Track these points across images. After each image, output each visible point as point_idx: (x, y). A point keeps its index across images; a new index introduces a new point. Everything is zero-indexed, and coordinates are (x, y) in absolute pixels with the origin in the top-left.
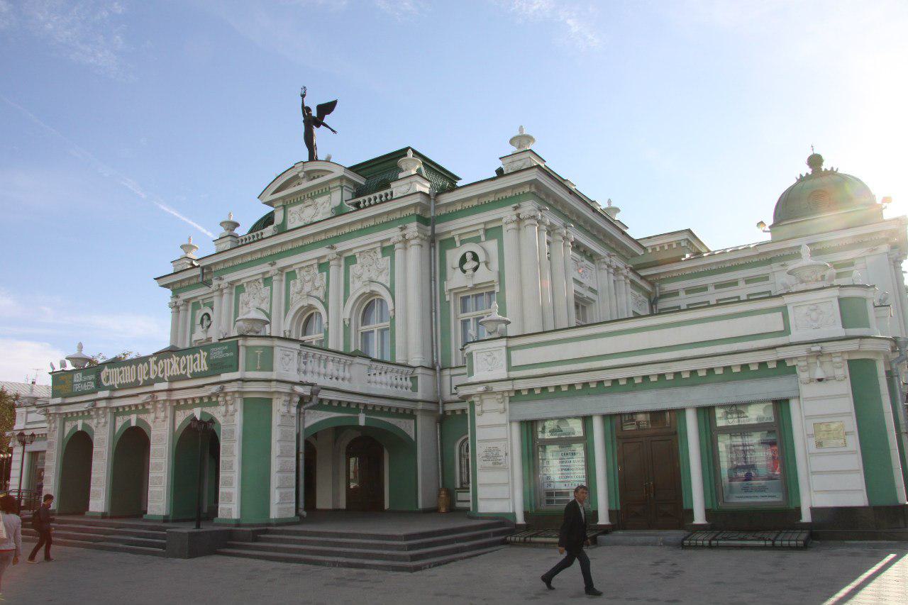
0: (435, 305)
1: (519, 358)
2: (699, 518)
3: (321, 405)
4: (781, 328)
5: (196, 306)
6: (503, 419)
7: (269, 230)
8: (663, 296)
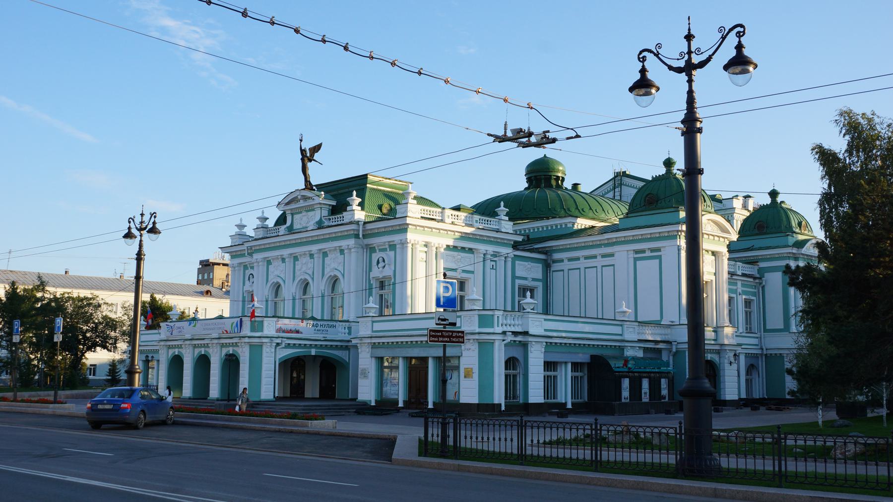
5: (246, 268)
7: (282, 229)
8: (555, 261)
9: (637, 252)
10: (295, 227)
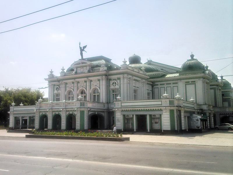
0: (108, 90)
1: (123, 104)
2: (149, 131)
3: (91, 111)
4: (161, 104)
6: (12, 116)
9: (186, 82)
10: (78, 72)
